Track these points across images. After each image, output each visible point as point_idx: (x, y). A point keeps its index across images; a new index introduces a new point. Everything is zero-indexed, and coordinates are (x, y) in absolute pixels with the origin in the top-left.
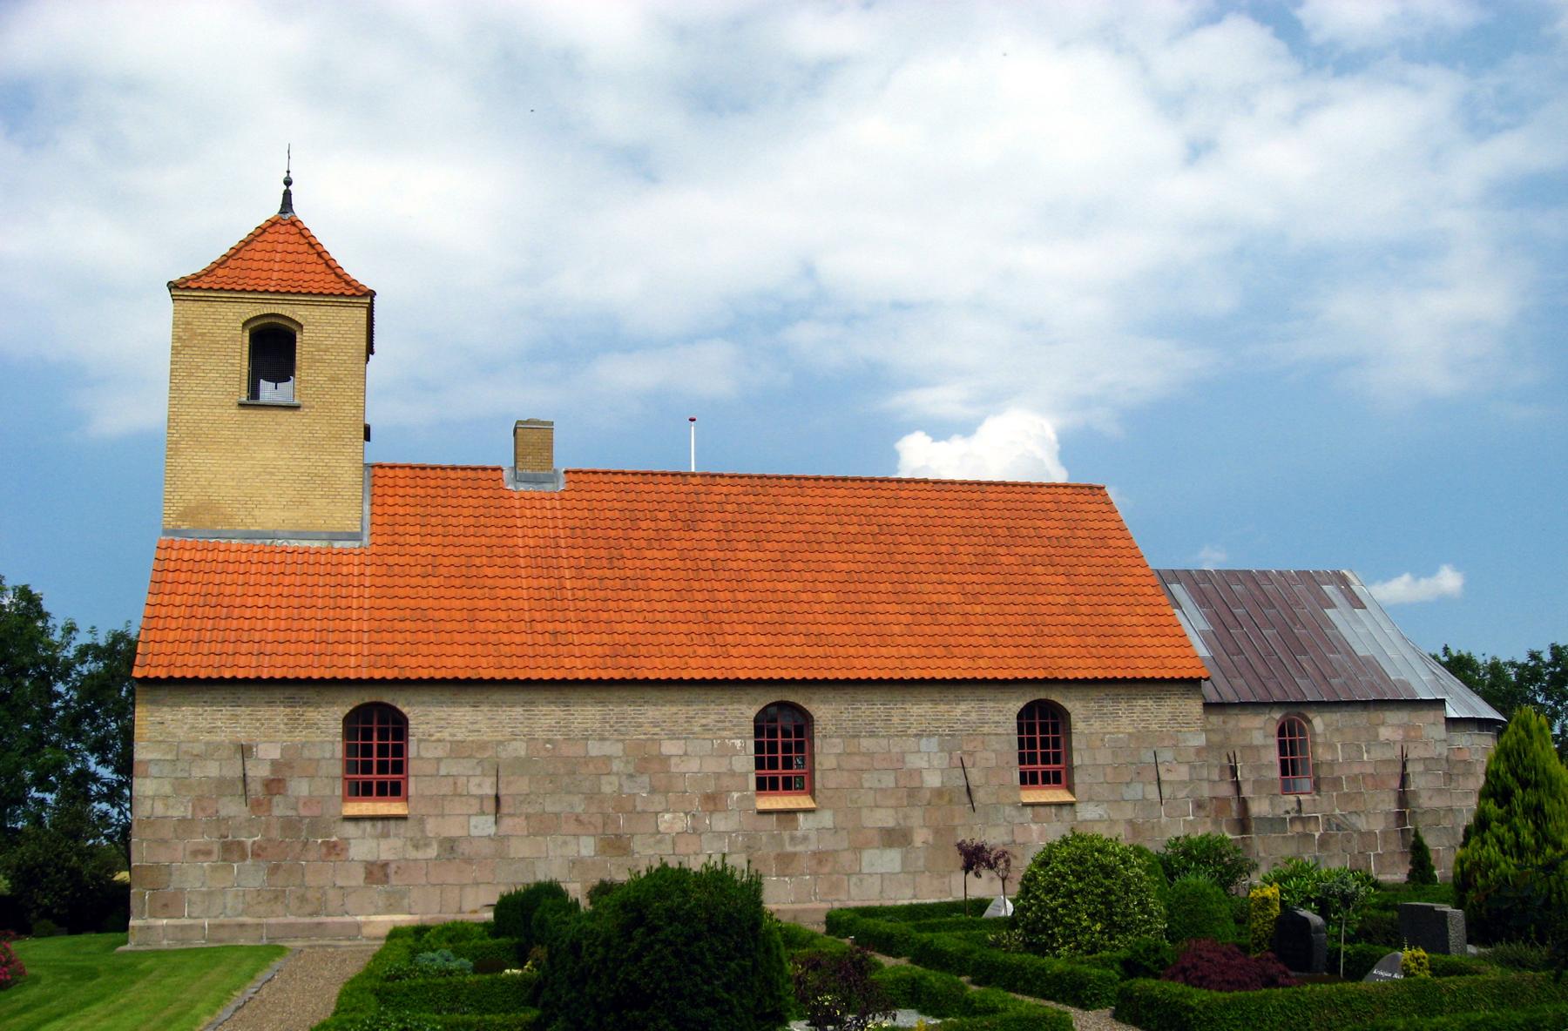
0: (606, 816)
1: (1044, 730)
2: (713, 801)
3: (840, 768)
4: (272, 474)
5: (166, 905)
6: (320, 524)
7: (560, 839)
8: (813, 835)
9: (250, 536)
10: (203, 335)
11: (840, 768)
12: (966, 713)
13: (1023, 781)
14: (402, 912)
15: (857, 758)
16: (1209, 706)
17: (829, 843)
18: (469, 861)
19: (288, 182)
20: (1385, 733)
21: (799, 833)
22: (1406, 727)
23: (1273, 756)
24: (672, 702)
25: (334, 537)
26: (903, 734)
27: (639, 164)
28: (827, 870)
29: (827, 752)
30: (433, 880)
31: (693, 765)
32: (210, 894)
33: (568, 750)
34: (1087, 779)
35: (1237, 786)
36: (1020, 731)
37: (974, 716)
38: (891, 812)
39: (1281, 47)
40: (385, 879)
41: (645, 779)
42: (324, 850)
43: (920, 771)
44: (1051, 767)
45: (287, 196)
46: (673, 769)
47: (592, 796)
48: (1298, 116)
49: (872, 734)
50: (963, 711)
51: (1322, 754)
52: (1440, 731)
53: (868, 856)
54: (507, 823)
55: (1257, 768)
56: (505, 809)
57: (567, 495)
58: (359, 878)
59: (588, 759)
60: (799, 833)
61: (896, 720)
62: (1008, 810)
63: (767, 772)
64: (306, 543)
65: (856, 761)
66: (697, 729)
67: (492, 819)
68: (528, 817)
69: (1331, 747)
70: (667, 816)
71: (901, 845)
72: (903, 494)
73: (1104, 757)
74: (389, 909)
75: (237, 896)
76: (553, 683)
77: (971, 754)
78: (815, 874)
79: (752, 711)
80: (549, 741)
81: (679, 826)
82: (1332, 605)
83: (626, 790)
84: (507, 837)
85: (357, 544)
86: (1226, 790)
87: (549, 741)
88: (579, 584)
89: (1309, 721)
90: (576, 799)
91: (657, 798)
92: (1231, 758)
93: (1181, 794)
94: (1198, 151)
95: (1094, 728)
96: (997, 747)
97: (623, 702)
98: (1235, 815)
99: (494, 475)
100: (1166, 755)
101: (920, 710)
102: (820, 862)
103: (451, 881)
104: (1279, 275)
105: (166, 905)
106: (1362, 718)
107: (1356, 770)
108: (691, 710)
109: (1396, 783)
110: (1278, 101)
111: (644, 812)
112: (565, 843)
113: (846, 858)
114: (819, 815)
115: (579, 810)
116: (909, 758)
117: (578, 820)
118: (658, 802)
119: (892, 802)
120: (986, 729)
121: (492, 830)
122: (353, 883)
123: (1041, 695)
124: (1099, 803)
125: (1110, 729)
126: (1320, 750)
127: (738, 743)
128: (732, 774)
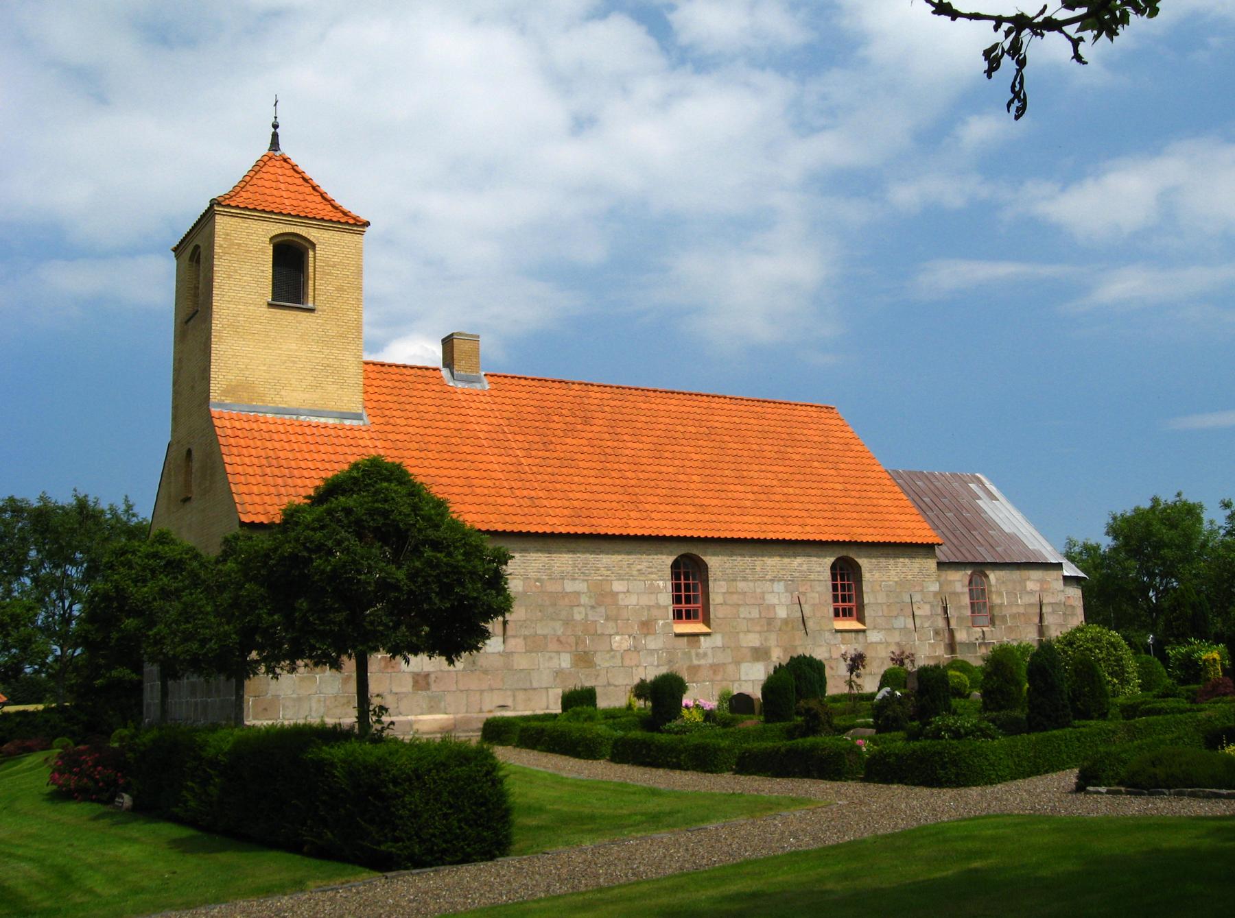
0: (578, 638)
1: (842, 579)
2: (647, 626)
3: (725, 603)
4: (294, 362)
5: (265, 709)
6: (332, 406)
7: (547, 655)
8: (710, 652)
9: (278, 411)
10: (239, 245)
11: (725, 603)
12: (801, 565)
13: (837, 614)
14: (439, 713)
15: (735, 596)
16: (941, 565)
17: (721, 658)
18: (486, 672)
19: (275, 126)
20: (1031, 585)
21: (701, 651)
22: (1042, 582)
23: (966, 600)
24: (619, 553)
25: (343, 416)
26: (762, 579)
27: (90, 84)
28: (719, 677)
29: (717, 591)
30: (461, 687)
31: (633, 600)
32: (299, 699)
33: (551, 587)
34: (873, 613)
35: (948, 620)
36: (834, 577)
37: (805, 567)
38: (757, 636)
39: (652, 43)
40: (427, 687)
41: (602, 610)
42: (383, 664)
43: (774, 606)
44: (847, 605)
45: (275, 136)
46: (621, 603)
47: (568, 622)
48: (666, 103)
49: (745, 579)
50: (799, 563)
51: (996, 600)
52: (1060, 584)
53: (745, 667)
54: (512, 642)
55: (960, 607)
56: (509, 632)
57: (493, 393)
58: (407, 686)
59: (565, 594)
60: (701, 651)
61: (758, 569)
62: (827, 635)
63: (683, 606)
64: (323, 420)
65: (735, 598)
66: (635, 573)
67: (501, 639)
68: (525, 638)
69: (1000, 594)
70: (618, 638)
71: (764, 660)
72: (713, 405)
73: (881, 598)
74: (431, 710)
75: (319, 701)
76: (544, 536)
77: (804, 594)
78: (712, 681)
79: (670, 560)
80: (538, 580)
81: (625, 645)
82: (979, 498)
83: (590, 618)
84: (512, 653)
85: (361, 423)
86: (941, 623)
87: (538, 580)
88: (530, 461)
89: (987, 576)
90: (558, 625)
91: (611, 624)
92: (944, 601)
93: (926, 625)
94: (582, 124)
95: (878, 576)
96: (819, 589)
97: (587, 551)
98: (947, 641)
99: (435, 374)
100: (917, 598)
101: (772, 563)
102: (715, 672)
103: (473, 687)
104: (643, 234)
105: (265, 709)
106: (1016, 575)
107: (1014, 610)
108: (631, 558)
109: (1037, 620)
110: (649, 88)
111: (603, 634)
112: (551, 658)
113: (731, 669)
114: (713, 637)
115: (559, 633)
116: (767, 596)
117: (559, 640)
118: (610, 628)
119: (758, 628)
120: (812, 577)
121: (501, 648)
122: (404, 690)
123: (843, 553)
124: (880, 630)
125: (885, 578)
126: (994, 597)
127: (661, 583)
128: (658, 606)
